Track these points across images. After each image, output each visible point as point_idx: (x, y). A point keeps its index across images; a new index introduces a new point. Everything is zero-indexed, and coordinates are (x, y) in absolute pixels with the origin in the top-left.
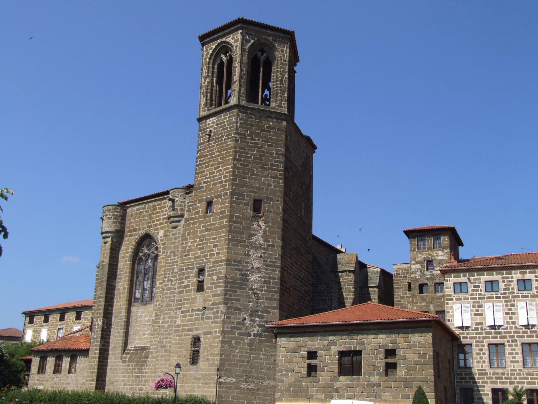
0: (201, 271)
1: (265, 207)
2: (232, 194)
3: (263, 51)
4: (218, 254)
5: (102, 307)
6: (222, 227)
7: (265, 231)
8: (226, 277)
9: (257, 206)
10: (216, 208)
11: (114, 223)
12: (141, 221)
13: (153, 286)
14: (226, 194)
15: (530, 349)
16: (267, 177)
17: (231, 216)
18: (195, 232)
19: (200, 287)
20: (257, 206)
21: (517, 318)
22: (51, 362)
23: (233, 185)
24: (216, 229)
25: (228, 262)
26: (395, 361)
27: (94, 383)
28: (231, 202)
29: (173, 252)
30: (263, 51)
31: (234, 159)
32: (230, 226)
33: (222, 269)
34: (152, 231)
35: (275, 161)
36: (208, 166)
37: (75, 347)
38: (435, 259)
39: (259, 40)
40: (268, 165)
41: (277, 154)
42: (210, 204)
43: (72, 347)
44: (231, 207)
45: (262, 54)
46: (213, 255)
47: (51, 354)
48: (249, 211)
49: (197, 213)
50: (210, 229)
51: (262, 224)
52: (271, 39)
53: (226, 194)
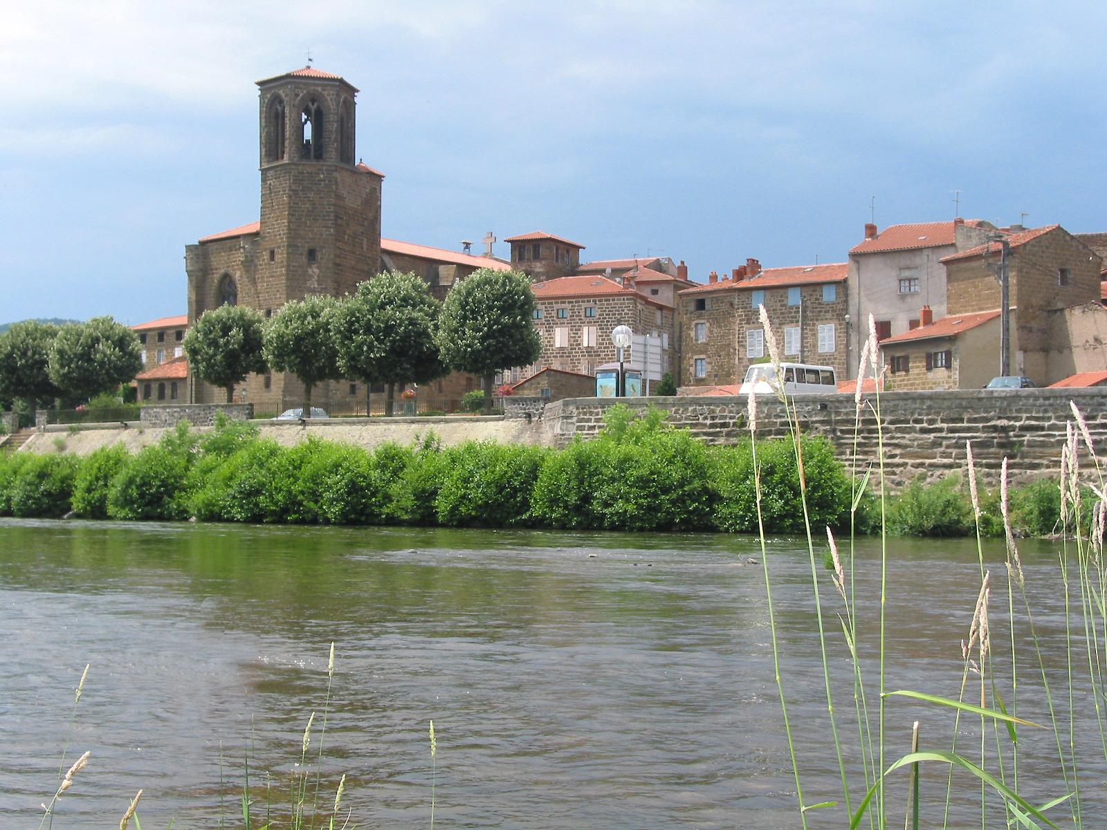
1: (319, 255)
2: (289, 246)
3: (313, 101)
4: (280, 298)
6: (282, 276)
7: (318, 276)
9: (312, 254)
10: (277, 257)
11: (197, 262)
12: (220, 260)
14: (283, 246)
15: (230, 399)
16: (319, 227)
17: (288, 266)
18: (263, 278)
20: (312, 254)
21: (554, 342)
22: (442, 505)
23: (288, 238)
24: (278, 276)
28: (288, 253)
29: (247, 293)
30: (313, 101)
31: (289, 214)
32: (288, 275)
34: (231, 272)
35: (327, 212)
36: (269, 218)
37: (174, 375)
38: (533, 271)
39: (308, 92)
40: (319, 216)
41: (328, 205)
42: (272, 253)
43: (171, 376)
44: (288, 258)
45: (313, 104)
46: (276, 298)
48: (304, 259)
49: (263, 260)
50: (274, 276)
51: (317, 271)
52: (320, 89)
53: (283, 246)
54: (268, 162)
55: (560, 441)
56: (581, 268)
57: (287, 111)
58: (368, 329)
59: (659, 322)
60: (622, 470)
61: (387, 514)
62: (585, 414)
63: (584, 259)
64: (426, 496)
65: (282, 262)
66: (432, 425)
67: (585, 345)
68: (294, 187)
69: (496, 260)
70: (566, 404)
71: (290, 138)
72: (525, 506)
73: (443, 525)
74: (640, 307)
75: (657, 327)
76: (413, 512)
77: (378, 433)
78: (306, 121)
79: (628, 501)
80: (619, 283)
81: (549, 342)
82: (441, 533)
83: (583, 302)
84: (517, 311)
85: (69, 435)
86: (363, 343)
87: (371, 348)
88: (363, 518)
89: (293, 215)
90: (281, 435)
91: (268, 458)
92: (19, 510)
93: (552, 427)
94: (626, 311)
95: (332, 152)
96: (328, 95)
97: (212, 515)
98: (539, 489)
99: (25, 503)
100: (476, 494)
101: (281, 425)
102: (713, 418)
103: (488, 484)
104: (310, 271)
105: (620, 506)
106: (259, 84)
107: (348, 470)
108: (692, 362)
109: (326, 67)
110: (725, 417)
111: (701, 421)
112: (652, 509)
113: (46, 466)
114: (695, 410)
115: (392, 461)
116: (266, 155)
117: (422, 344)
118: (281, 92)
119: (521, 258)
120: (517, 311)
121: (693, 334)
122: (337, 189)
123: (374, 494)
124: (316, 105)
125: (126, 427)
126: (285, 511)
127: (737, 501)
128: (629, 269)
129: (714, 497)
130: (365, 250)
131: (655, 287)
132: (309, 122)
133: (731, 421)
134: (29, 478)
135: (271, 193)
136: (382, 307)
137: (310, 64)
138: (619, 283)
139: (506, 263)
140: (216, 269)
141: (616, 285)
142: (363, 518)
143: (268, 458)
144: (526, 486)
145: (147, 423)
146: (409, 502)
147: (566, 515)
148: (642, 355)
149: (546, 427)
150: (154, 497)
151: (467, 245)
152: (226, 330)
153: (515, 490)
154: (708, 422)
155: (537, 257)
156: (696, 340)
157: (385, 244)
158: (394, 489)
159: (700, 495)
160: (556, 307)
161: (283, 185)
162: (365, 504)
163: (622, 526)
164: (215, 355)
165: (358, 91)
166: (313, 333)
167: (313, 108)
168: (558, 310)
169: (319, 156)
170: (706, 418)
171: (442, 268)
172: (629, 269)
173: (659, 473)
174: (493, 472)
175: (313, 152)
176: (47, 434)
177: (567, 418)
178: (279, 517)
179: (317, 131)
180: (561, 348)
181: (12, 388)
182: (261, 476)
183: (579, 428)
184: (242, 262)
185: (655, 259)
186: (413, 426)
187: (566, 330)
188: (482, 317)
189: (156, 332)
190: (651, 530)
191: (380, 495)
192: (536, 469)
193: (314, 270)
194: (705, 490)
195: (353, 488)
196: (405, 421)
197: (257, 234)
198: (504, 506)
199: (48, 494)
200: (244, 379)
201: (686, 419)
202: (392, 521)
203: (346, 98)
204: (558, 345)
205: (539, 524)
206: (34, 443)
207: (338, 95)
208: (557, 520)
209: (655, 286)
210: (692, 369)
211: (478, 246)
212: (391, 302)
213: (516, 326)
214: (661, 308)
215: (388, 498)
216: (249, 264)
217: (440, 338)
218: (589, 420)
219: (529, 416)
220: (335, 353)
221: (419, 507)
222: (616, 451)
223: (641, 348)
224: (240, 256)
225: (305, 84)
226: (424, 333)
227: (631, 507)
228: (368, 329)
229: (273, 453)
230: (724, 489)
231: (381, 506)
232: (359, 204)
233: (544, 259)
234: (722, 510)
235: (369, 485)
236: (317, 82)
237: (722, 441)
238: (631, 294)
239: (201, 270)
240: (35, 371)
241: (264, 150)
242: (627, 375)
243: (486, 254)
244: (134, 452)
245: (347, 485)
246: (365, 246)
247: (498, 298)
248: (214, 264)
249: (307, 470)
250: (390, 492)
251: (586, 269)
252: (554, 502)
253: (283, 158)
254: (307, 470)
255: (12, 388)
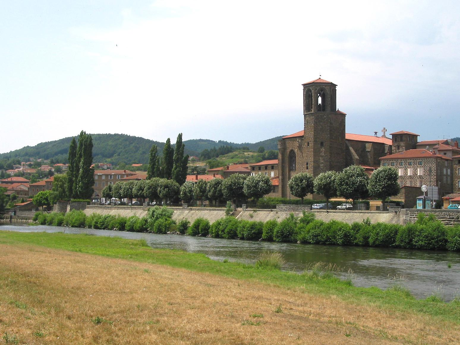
0: (307, 164)
1: (324, 144)
3: (322, 91)
5: (281, 173)
8: (313, 166)
9: (322, 144)
11: (282, 146)
13: (295, 166)
17: (314, 148)
18: (305, 152)
19: (307, 169)
20: (322, 144)
22: (371, 241)
23: (314, 138)
24: (310, 152)
25: (314, 162)
26: (278, 191)
27: (281, 195)
28: (314, 144)
30: (322, 91)
33: (312, 163)
44: (314, 145)
47: (282, 206)
48: (319, 145)
51: (324, 149)
52: (324, 86)
54: (307, 112)
55: (405, 221)
56: (418, 144)
57: (313, 95)
58: (347, 184)
59: (446, 165)
60: (421, 233)
61: (355, 243)
62: (412, 213)
63: (419, 140)
64: (366, 238)
65: (312, 147)
66: (367, 214)
67: (419, 175)
68: (315, 121)
69: (386, 138)
70: (407, 210)
71: (314, 104)
72: (394, 241)
73: (371, 246)
74: (439, 161)
75: (446, 167)
76: (363, 242)
77: (351, 216)
78: (319, 96)
79: (422, 241)
80: (431, 152)
81: (406, 173)
82: (371, 250)
83: (418, 159)
84: (393, 180)
85: (253, 213)
86: (345, 189)
87: (347, 190)
88: (349, 244)
89: (315, 131)
90: (321, 216)
91: (320, 226)
92: (247, 237)
93: (403, 216)
94: (433, 163)
95: (328, 108)
96: (327, 88)
97: (305, 242)
98: (398, 236)
99: (248, 236)
100: (380, 238)
101: (320, 212)
102: (450, 216)
103: (384, 235)
104: (321, 150)
105: (420, 243)
106: (304, 85)
107: (344, 230)
108: (457, 182)
109: (328, 78)
110: (453, 216)
111: (446, 217)
112: (429, 244)
113: (253, 225)
114: (444, 214)
115: (356, 227)
116: (306, 110)
117: (363, 188)
118: (311, 88)
119: (396, 140)
120: (393, 180)
121: (457, 172)
122: (330, 121)
123: (352, 237)
124: (323, 92)
125: (272, 211)
126: (326, 241)
127: (452, 243)
128: (435, 145)
129: (446, 241)
130: (340, 141)
131: (445, 152)
132: (320, 97)
133: (455, 217)
134: (249, 229)
135: (307, 123)
136: (351, 177)
137: (320, 77)
138: (431, 152)
139: (390, 139)
140: (288, 148)
141: (429, 152)
142: (349, 244)
143: (320, 226)
144: (394, 237)
145: (279, 210)
146: (361, 239)
147: (405, 245)
148: (431, 192)
149: (401, 216)
150: (286, 235)
151: (376, 133)
152: (301, 180)
153: (392, 237)
154: (448, 217)
155: (401, 140)
156: (459, 174)
157: (347, 137)
158: (358, 235)
159: (442, 240)
160: (408, 161)
161: (312, 119)
162: (349, 240)
163: (421, 249)
164: (298, 188)
165: (337, 85)
166: (330, 183)
167: (322, 93)
168: (409, 162)
169: (324, 110)
170: (447, 216)
171: (367, 145)
172: (435, 145)
173: (431, 234)
174: (385, 232)
175: (321, 108)
176: (246, 212)
177: (407, 214)
178: (324, 244)
179: (323, 100)
180: (410, 176)
181: (231, 195)
182: (318, 231)
183: (410, 218)
184: (298, 146)
185: (446, 140)
186: (361, 214)
187: (412, 169)
188: (382, 182)
189: (264, 166)
190: (429, 249)
191: (353, 238)
192: (397, 232)
193: (323, 149)
194: (444, 239)
195: (346, 235)
196: (359, 212)
197: (303, 136)
198: (389, 243)
199: (254, 233)
200: (307, 195)
201: (442, 216)
202: (357, 245)
203: (333, 89)
204: (409, 175)
205: (398, 247)
206: (242, 215)
207: (330, 88)
208: (403, 246)
209: (445, 152)
210: (457, 184)
211: (380, 134)
212: (354, 175)
213: (392, 184)
214: (447, 160)
215: (356, 238)
216: (300, 147)
217: (369, 187)
218: (413, 215)
219: (396, 212)
220: (336, 190)
221: (364, 241)
222: (420, 227)
223: (431, 190)
224: (297, 144)
225: (319, 85)
226: (364, 185)
227: (423, 243)
228: (347, 184)
229: (322, 224)
230: (450, 239)
231: (353, 241)
232: (338, 125)
233: (404, 141)
234: (448, 245)
235: (350, 235)
236: (323, 84)
237: (452, 223)
238: (435, 157)
239: (283, 148)
240: (238, 190)
241: (305, 108)
242: (426, 200)
243: (383, 136)
244: (279, 221)
245: (344, 234)
246: (340, 140)
247: (387, 176)
248: (288, 145)
249: (332, 229)
250: (356, 236)
251: (420, 144)
252: (402, 241)
253: (311, 111)
254: (332, 229)
255: (231, 195)
